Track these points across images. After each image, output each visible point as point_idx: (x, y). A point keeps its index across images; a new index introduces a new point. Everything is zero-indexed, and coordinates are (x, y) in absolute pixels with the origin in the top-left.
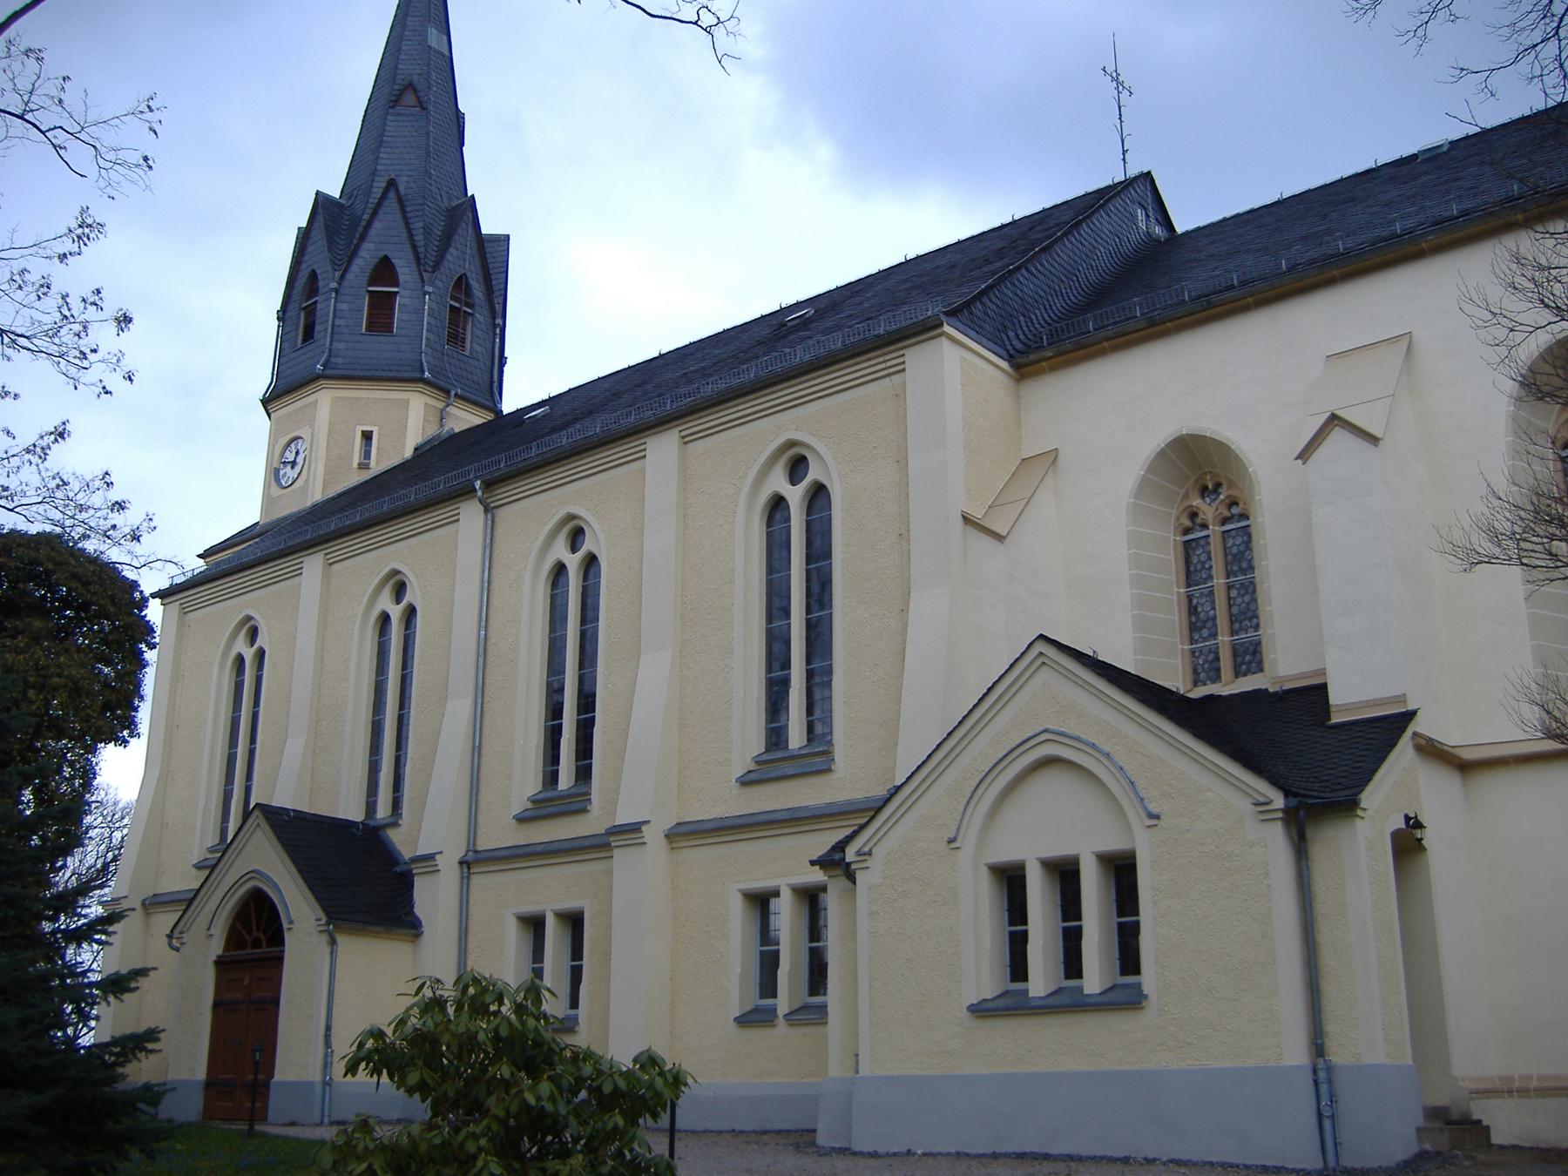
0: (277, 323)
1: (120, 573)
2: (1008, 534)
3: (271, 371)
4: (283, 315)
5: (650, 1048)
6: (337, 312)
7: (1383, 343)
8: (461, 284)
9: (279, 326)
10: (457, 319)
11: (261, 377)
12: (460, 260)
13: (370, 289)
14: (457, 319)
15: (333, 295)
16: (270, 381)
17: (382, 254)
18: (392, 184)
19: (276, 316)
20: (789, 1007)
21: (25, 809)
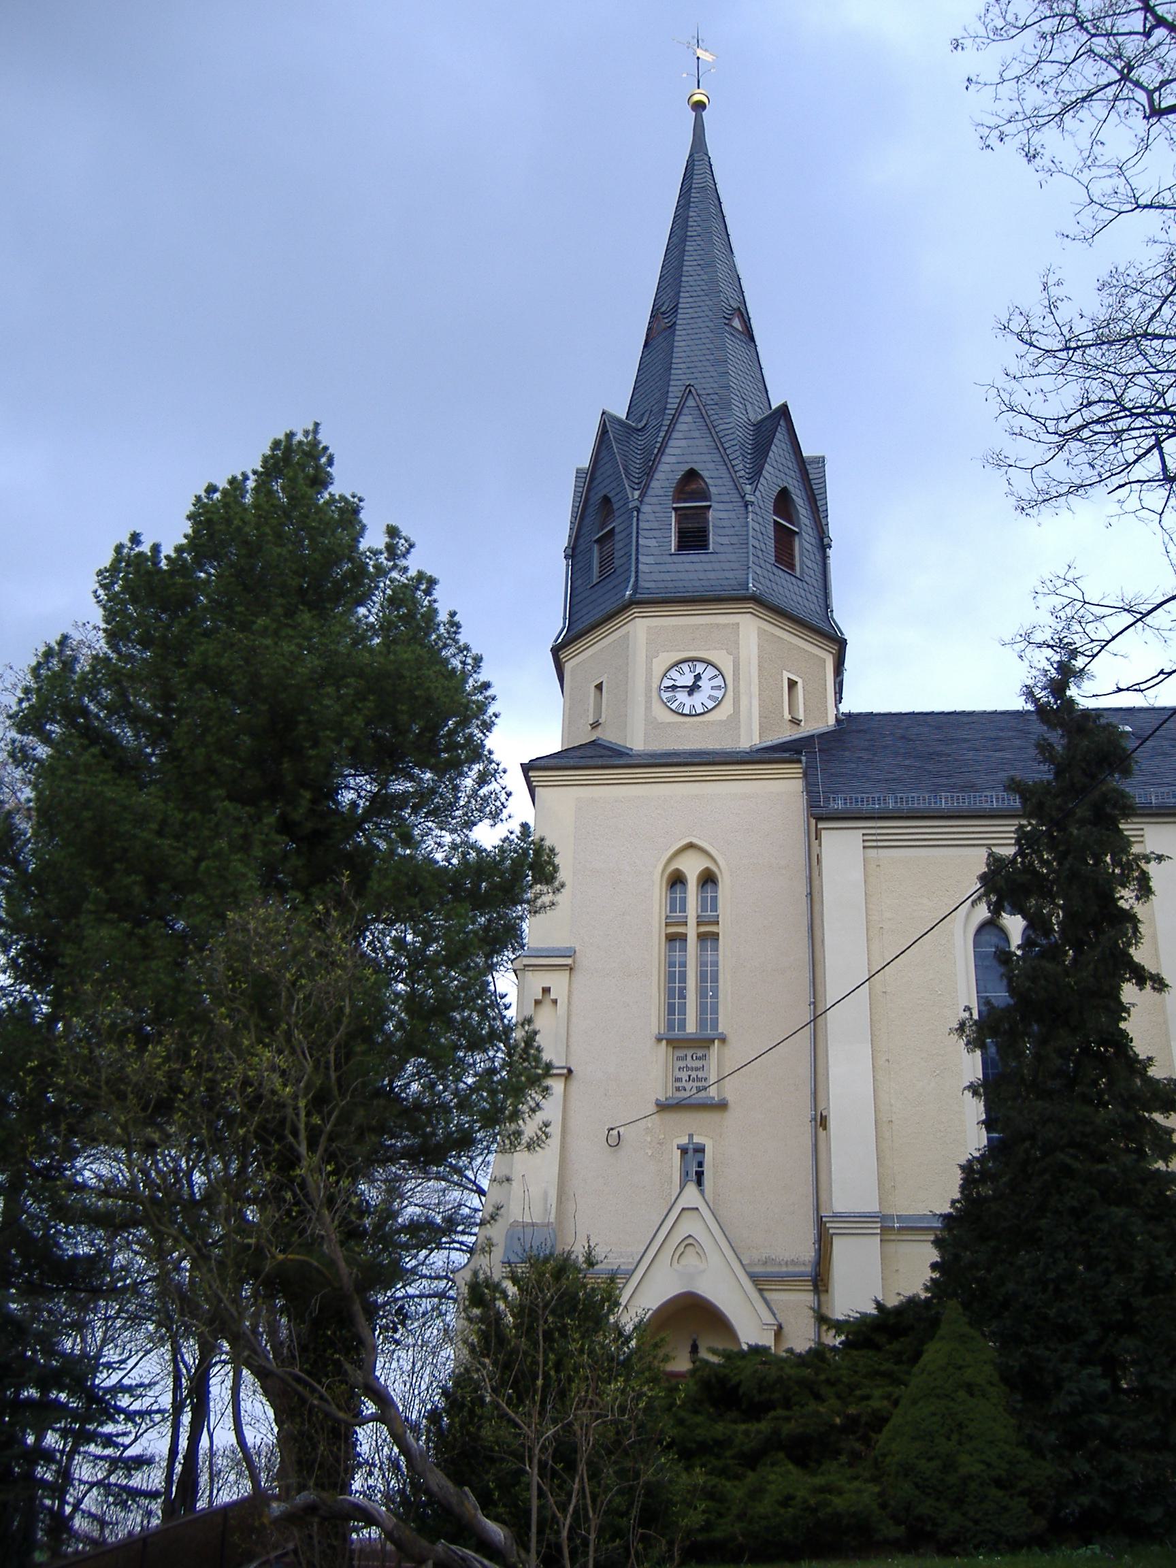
0: (565, 562)
1: (1143, 1073)
2: (813, 863)
3: (562, 615)
4: (573, 553)
5: (961, 1166)
6: (640, 574)
7: (563, 954)
8: (783, 498)
9: (568, 565)
10: (784, 539)
11: (553, 623)
12: (778, 472)
13: (675, 505)
14: (784, 539)
15: (635, 513)
16: (561, 625)
17: (687, 467)
18: (688, 390)
19: (563, 554)
20: (826, 1018)
21: (491, 1026)
